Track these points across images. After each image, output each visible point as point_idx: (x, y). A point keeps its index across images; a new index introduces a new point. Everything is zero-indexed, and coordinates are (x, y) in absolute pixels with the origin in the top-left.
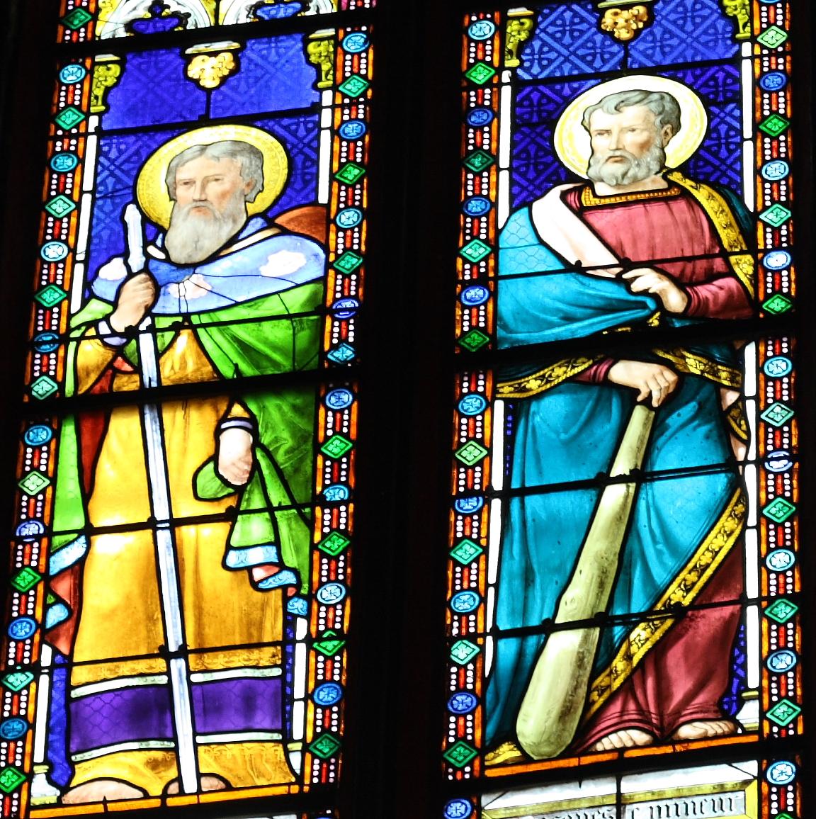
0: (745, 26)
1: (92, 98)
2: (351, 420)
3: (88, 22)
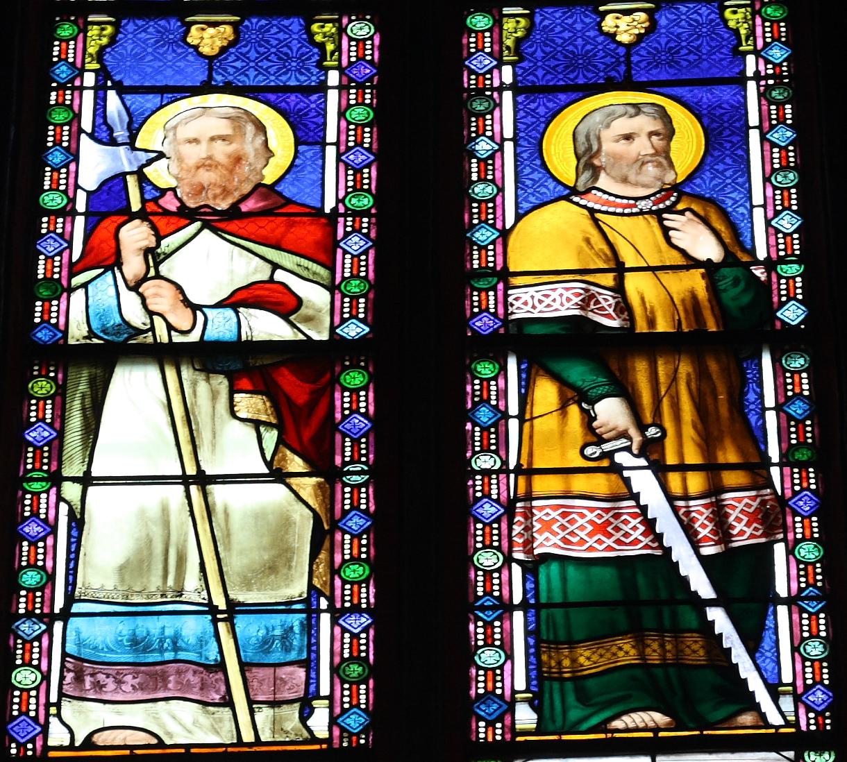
0: (747, 39)
1: (87, 56)
2: (367, 402)
3: (37, 735)
